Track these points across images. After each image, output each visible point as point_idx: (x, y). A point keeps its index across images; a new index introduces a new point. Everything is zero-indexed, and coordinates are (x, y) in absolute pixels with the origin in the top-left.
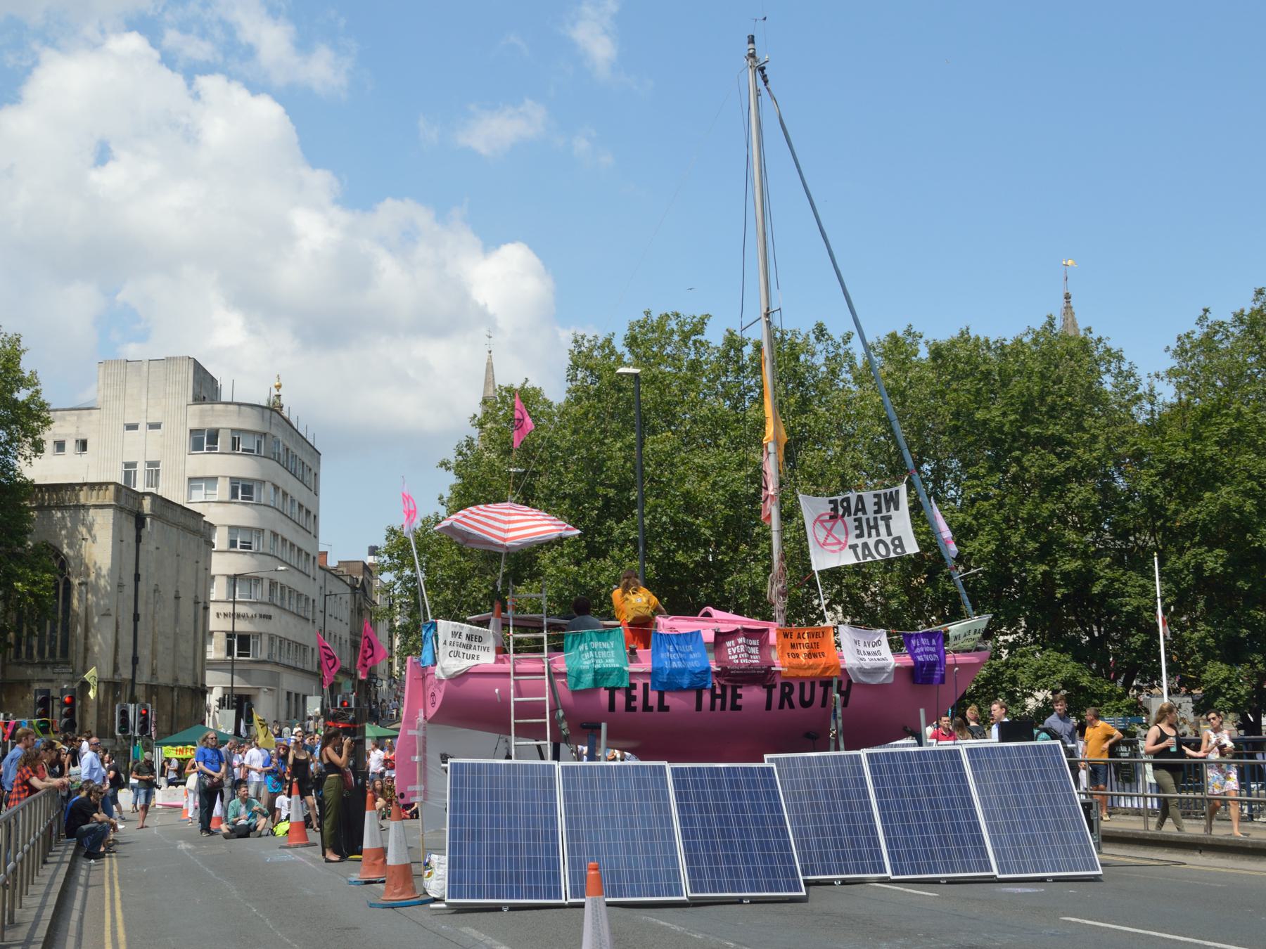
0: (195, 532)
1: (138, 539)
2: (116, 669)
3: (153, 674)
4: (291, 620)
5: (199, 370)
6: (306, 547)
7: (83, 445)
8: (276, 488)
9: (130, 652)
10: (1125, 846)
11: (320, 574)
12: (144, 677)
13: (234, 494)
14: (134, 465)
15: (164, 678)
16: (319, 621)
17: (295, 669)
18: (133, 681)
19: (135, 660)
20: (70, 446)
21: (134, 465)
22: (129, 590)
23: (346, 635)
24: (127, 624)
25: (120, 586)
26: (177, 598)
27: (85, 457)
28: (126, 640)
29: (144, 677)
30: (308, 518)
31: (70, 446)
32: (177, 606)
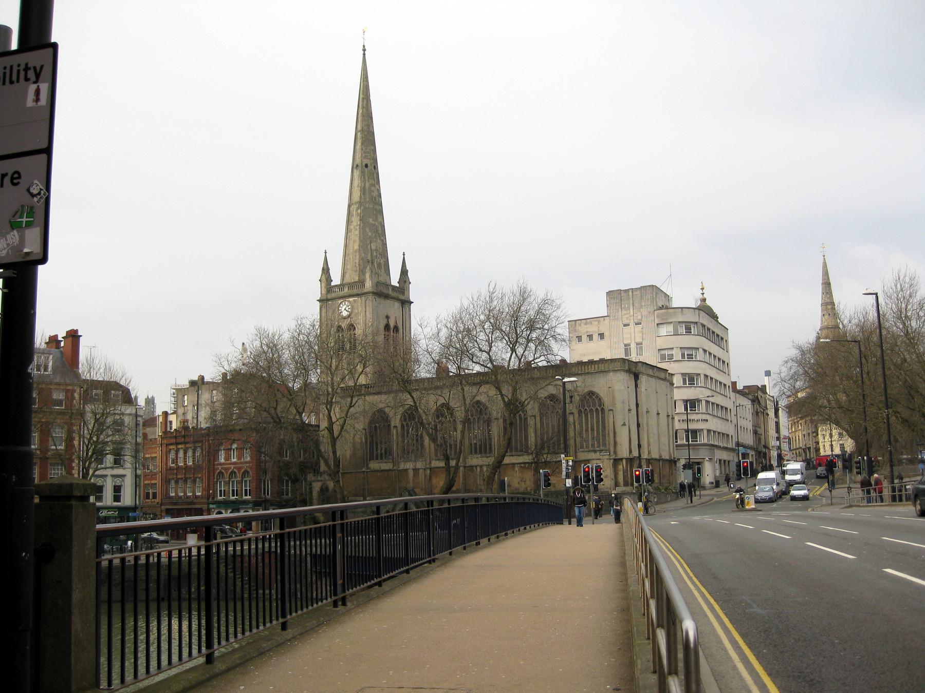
0: (664, 379)
1: (636, 386)
2: (631, 451)
3: (649, 453)
7: (602, 336)
8: (705, 351)
12: (645, 456)
14: (629, 345)
15: (655, 455)
19: (639, 446)
20: (595, 337)
21: (629, 345)
22: (634, 412)
23: (750, 426)
31: (595, 337)
32: (658, 418)
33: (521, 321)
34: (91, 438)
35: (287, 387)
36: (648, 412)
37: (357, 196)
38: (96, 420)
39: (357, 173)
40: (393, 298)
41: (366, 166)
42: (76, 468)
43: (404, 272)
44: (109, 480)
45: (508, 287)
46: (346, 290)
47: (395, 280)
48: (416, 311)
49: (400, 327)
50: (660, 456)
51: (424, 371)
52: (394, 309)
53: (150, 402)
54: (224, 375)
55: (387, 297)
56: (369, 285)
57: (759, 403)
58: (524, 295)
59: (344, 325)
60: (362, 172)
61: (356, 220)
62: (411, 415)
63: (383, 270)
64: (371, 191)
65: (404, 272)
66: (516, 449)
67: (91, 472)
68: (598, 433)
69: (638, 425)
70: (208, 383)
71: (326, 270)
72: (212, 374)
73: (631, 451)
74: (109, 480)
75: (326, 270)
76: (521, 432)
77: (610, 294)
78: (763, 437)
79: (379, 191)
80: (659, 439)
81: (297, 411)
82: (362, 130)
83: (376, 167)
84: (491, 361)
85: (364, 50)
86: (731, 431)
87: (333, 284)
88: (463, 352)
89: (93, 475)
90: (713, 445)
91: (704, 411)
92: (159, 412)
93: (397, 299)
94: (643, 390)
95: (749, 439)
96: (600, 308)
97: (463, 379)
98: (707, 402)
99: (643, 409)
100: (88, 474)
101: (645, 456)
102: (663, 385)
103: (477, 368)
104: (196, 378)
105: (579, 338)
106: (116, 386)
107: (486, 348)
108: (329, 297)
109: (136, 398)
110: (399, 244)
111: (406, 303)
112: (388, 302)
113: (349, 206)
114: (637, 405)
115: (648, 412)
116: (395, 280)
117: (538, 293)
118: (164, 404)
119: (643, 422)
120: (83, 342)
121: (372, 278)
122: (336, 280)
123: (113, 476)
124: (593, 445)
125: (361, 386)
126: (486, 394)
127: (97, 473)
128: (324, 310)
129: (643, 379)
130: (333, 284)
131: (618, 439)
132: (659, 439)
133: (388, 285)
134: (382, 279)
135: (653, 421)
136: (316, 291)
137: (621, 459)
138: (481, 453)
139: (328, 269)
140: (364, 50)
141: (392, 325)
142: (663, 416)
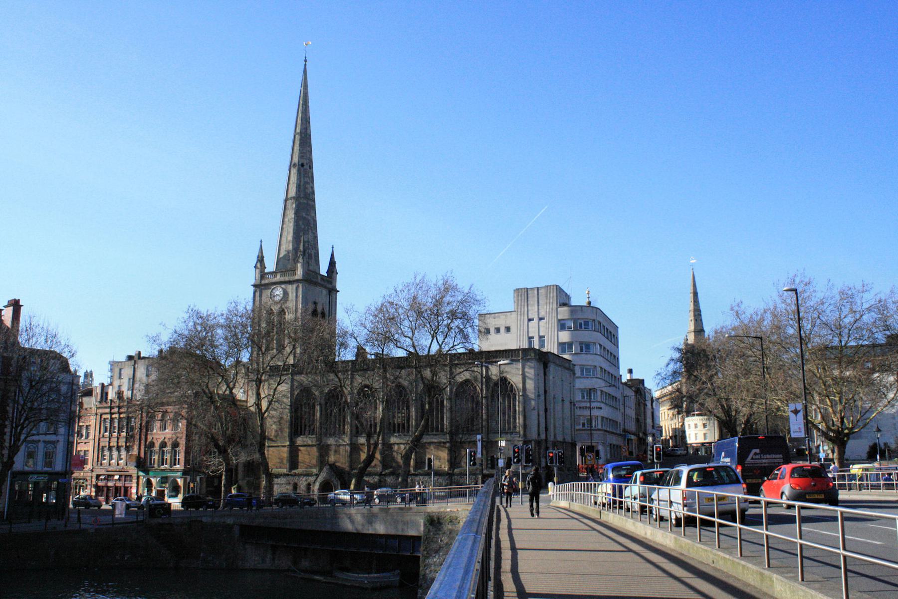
0: (568, 369)
1: (545, 374)
2: (539, 435)
3: (555, 436)
4: (611, 409)
5: (559, 290)
6: (615, 374)
7: (508, 329)
8: (601, 345)
9: (536, 422)
10: (877, 510)
11: (621, 386)
12: (551, 438)
13: (581, 350)
15: (560, 439)
16: (622, 410)
17: (613, 433)
18: (546, 440)
19: (546, 429)
20: (502, 330)
21: (533, 338)
22: (542, 398)
23: (634, 416)
24: (542, 413)
25: (539, 396)
26: (563, 400)
27: (508, 335)
28: (542, 420)
29: (551, 438)
30: (614, 360)
31: (502, 330)
32: (563, 405)
33: (444, 309)
34: (25, 404)
35: (218, 363)
36: (554, 398)
37: (293, 192)
38: (32, 387)
39: (294, 171)
40: (322, 286)
41: (302, 165)
42: (8, 434)
43: (332, 263)
44: (41, 445)
45: (434, 278)
46: (278, 277)
47: (323, 270)
48: (342, 300)
49: (327, 314)
50: (564, 439)
51: (348, 355)
52: (321, 295)
53: (89, 375)
54: (161, 351)
55: (316, 284)
56: (299, 273)
57: (641, 394)
58: (448, 288)
59: (276, 309)
60: (299, 170)
61: (291, 215)
62: (334, 397)
63: (313, 260)
64: (306, 188)
65: (332, 263)
66: (437, 430)
67: (22, 437)
68: (509, 417)
69: (546, 410)
70: (144, 358)
71: (261, 259)
72: (149, 350)
73: (539, 435)
74: (41, 445)
75: (261, 259)
76: (437, 414)
77: (517, 291)
78: (643, 425)
79: (313, 188)
80: (563, 423)
81: (228, 386)
82: (301, 133)
83: (311, 167)
84: (414, 346)
85: (306, 61)
86: (619, 419)
87: (266, 271)
88: (387, 338)
89: (25, 440)
90: (606, 431)
91: (599, 399)
92: (96, 383)
93: (325, 287)
94: (551, 378)
95: (632, 427)
96: (123, 359)
97: (383, 362)
98: (602, 391)
99: (551, 394)
100: (19, 440)
101: (551, 438)
102: (566, 374)
103: (401, 353)
104: (133, 354)
105: (488, 331)
106: (58, 357)
107: (410, 335)
108: (263, 282)
109: (76, 371)
110: (328, 238)
111: (333, 291)
112: (318, 289)
113: (286, 200)
114: (545, 392)
115: (554, 398)
116: (323, 270)
117: (463, 284)
118: (101, 377)
119: (551, 406)
120: (23, 311)
121: (305, 268)
122: (270, 266)
123: (44, 442)
124: (509, 428)
125: (288, 365)
126: (406, 378)
127: (28, 439)
128: (258, 294)
129: (552, 368)
130: (266, 271)
131: (527, 422)
132: (563, 423)
133: (317, 273)
134: (311, 268)
135: (559, 407)
136: (252, 277)
137: (531, 441)
138: (399, 431)
139: (262, 257)
140: (306, 61)
141: (319, 309)
142: (567, 403)
